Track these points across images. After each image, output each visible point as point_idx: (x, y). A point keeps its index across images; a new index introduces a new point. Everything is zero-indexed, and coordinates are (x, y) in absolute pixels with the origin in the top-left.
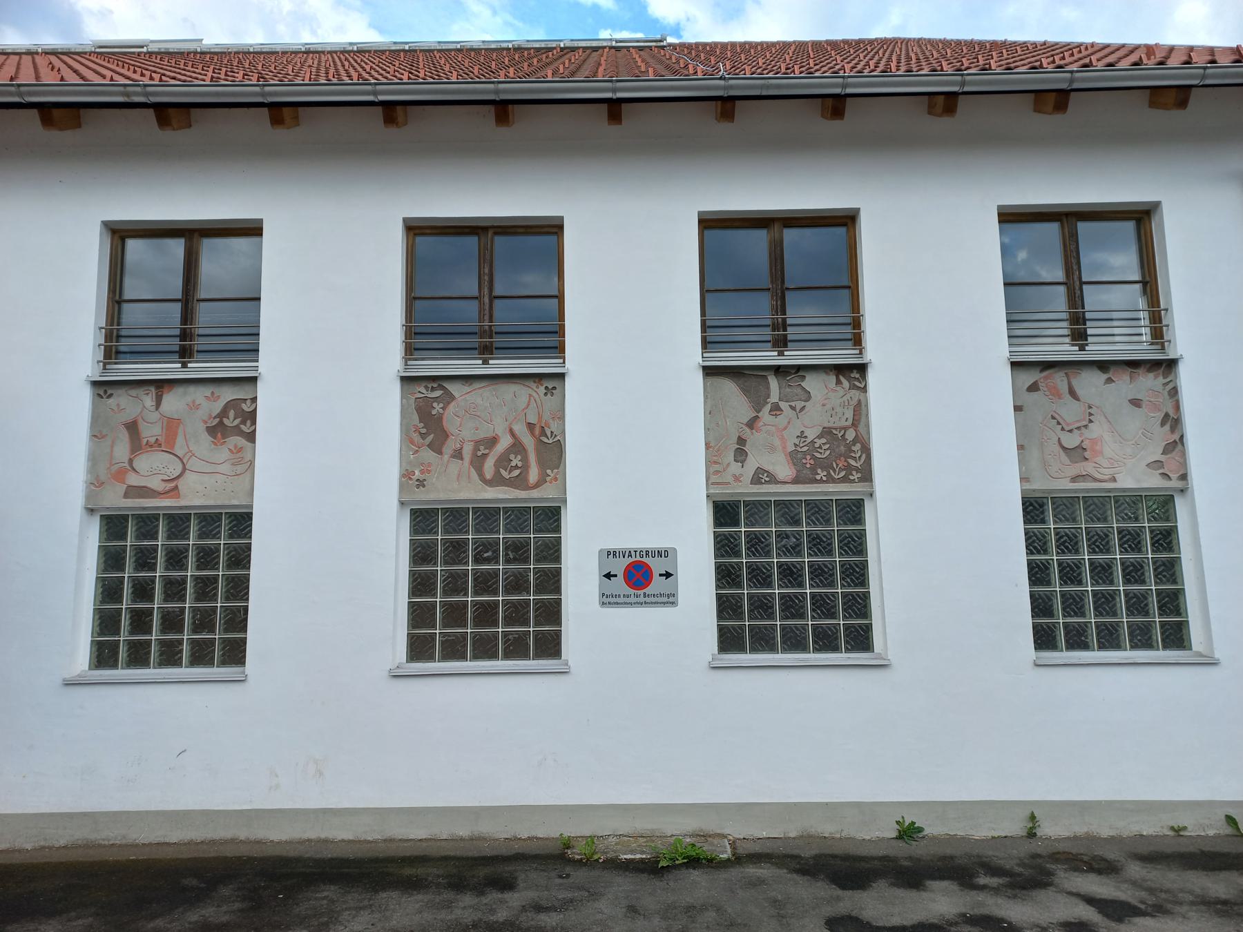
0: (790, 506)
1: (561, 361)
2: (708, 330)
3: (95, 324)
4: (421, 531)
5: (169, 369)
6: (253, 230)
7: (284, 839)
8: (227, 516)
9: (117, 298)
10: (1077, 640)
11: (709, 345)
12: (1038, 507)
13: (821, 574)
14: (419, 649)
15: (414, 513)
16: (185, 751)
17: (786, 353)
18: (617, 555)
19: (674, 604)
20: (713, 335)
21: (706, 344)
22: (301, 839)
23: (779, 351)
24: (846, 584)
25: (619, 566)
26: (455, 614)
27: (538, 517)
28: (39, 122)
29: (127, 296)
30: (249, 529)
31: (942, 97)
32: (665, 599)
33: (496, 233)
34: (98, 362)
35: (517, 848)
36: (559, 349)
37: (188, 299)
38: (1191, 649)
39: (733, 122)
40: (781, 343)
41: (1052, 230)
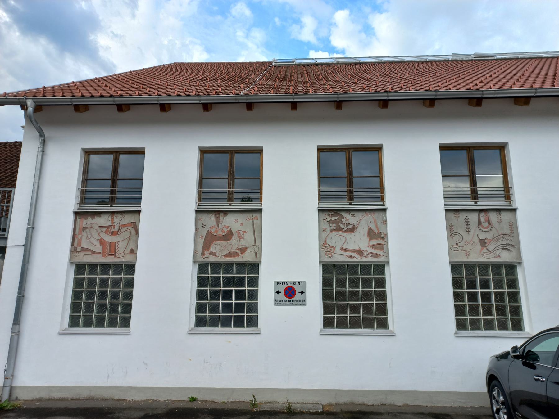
0: (367, 266)
1: (261, 204)
2: (321, 193)
3: (77, 187)
4: (226, 272)
5: (224, 206)
6: (141, 152)
7: (241, 400)
8: (100, 266)
9: (86, 178)
10: (475, 325)
11: (321, 199)
12: (485, 268)
13: (215, 295)
14: (200, 322)
15: (323, 264)
16: (390, 363)
17: (353, 203)
18: (282, 283)
19: (304, 305)
20: (204, 196)
21: (320, 199)
22: (60, 397)
23: (475, 202)
24: (377, 300)
25: (282, 288)
26: (368, 309)
27: (212, 268)
28: (74, 110)
29: (89, 178)
30: (133, 271)
31: (428, 101)
32: (301, 303)
33: (236, 153)
34: (77, 203)
35: (234, 407)
36: (138, 200)
37: (114, 180)
38: (524, 331)
39: (296, 110)
40: (351, 199)
41: (464, 153)
